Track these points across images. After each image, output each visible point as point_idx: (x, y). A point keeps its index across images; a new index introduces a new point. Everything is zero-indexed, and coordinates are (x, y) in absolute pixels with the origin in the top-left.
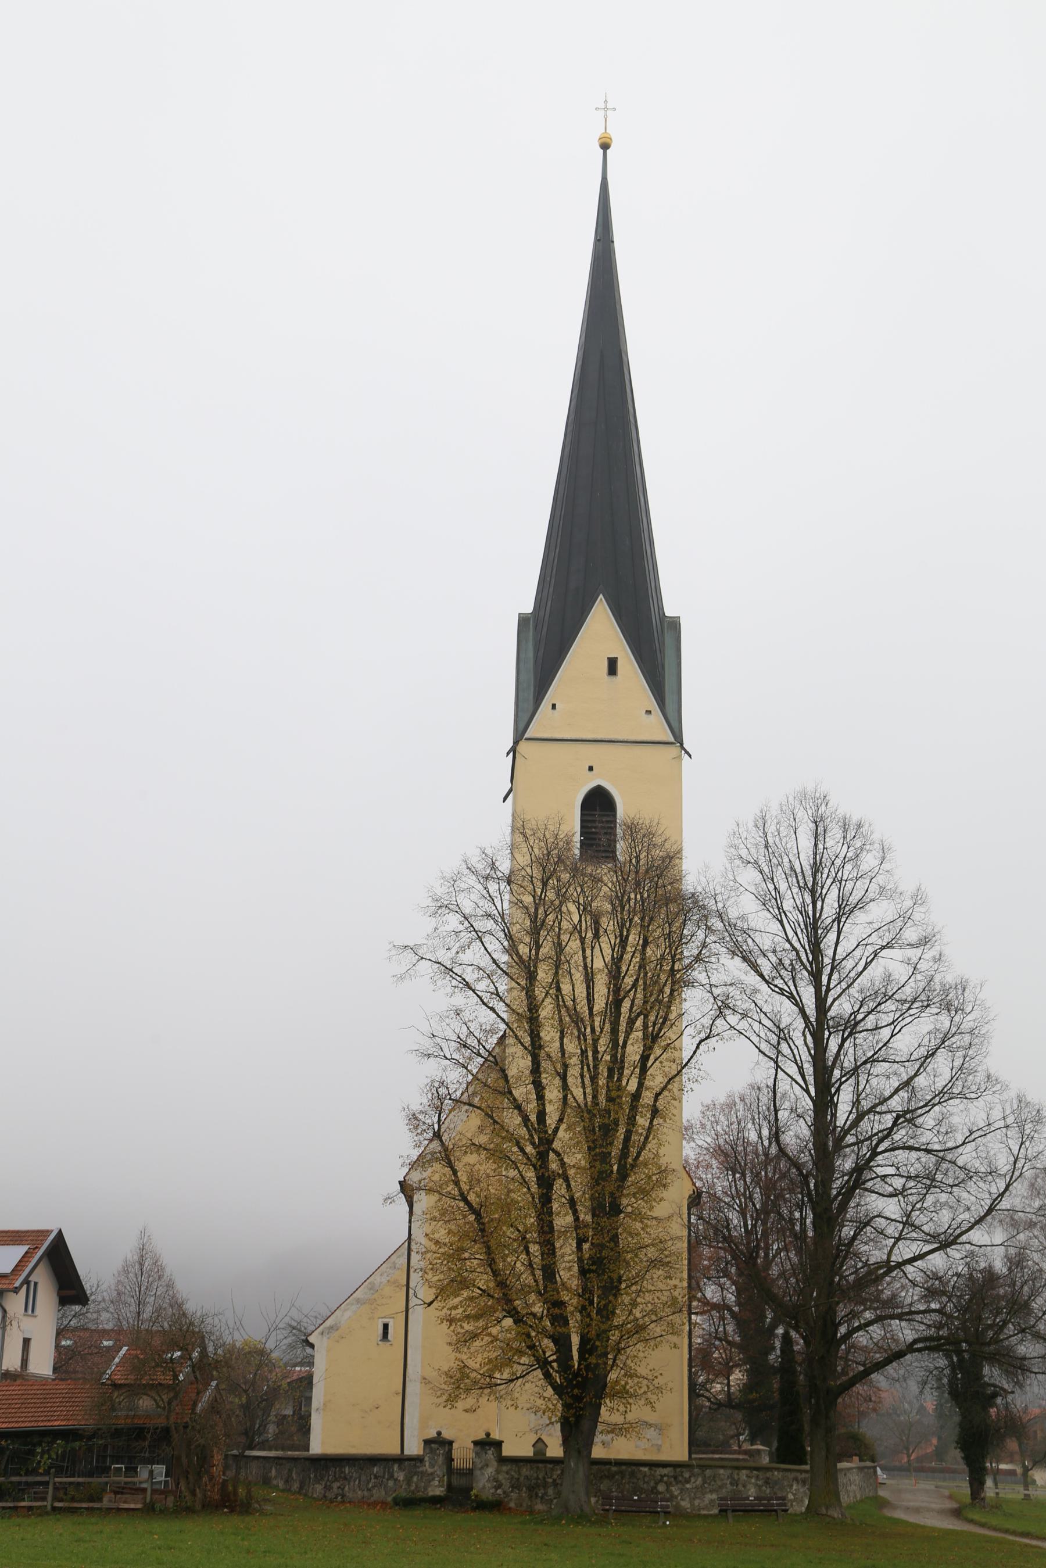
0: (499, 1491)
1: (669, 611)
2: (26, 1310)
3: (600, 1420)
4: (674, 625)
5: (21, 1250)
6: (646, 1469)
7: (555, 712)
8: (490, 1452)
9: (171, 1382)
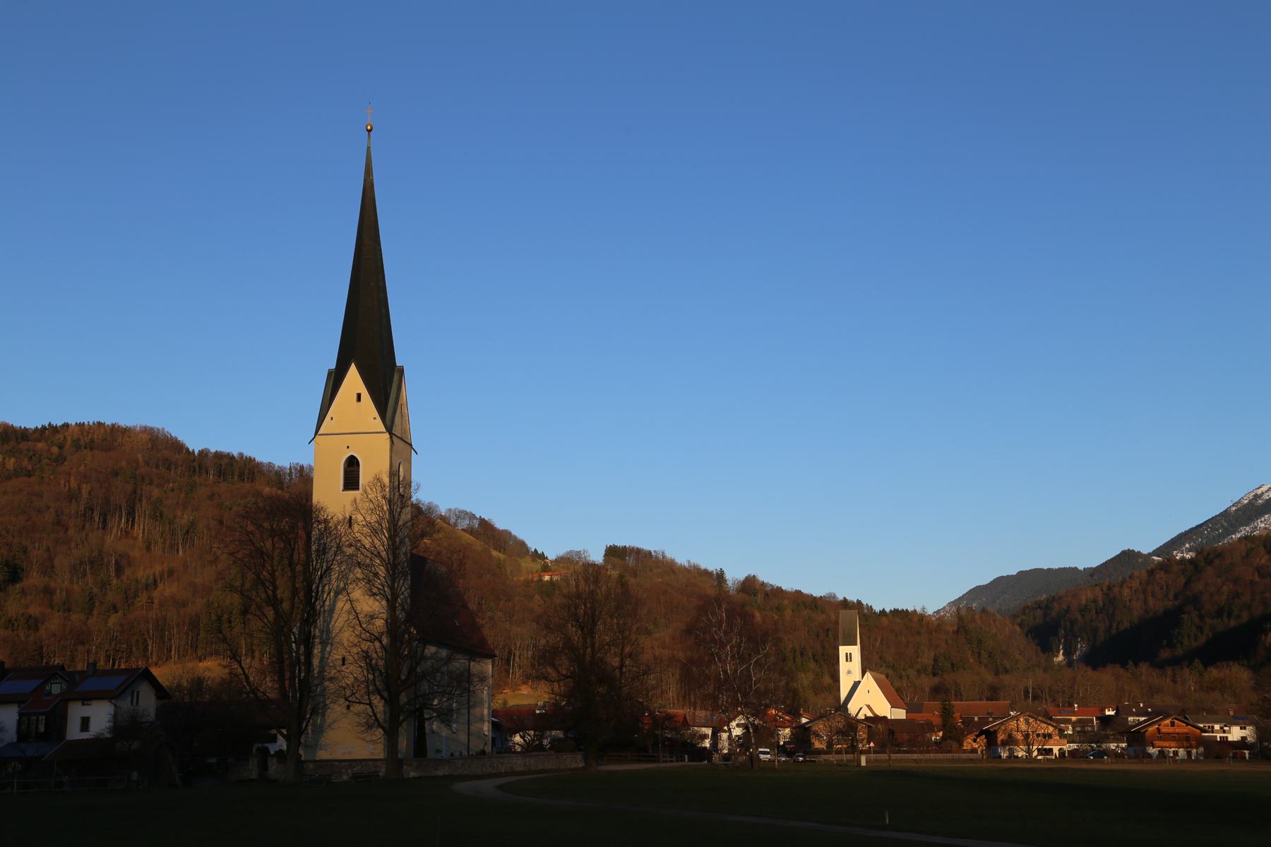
4: (401, 371)
6: (336, 763)
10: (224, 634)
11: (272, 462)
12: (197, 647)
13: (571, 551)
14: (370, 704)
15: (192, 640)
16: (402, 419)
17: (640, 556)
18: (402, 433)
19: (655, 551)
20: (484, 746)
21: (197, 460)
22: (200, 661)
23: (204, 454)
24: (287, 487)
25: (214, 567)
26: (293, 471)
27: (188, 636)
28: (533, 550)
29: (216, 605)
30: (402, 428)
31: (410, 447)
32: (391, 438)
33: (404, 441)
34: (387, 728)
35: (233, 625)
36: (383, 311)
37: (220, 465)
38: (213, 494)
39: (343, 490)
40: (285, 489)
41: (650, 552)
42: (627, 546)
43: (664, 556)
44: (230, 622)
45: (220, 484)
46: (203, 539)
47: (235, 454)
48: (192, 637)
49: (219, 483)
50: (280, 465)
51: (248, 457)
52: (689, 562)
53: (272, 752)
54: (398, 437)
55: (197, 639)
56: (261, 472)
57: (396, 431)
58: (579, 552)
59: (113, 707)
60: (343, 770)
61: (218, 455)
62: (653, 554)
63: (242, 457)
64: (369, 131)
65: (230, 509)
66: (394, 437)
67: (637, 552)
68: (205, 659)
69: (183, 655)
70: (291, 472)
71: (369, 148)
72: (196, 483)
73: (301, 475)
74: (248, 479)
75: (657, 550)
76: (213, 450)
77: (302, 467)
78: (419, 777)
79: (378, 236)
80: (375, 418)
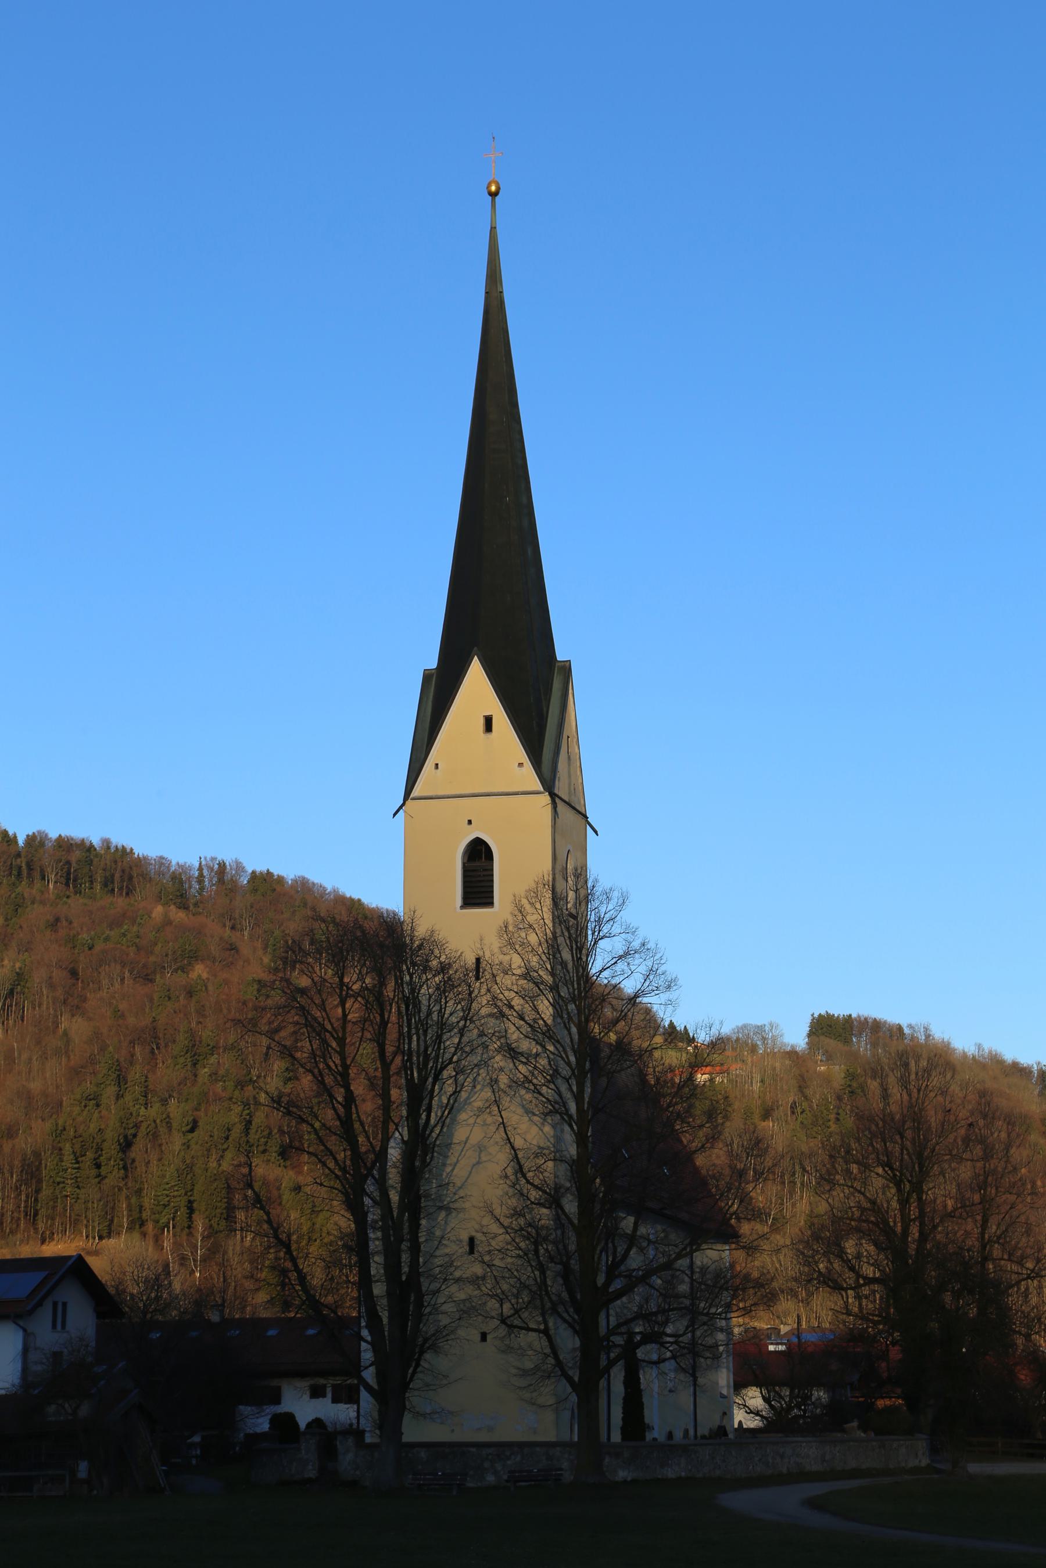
0: (358, 1473)
1: (561, 656)
2: (54, 1326)
3: (574, 1393)
4: (566, 670)
5: (39, 1276)
6: (473, 1450)
7: (438, 771)
8: (350, 1440)
9: (670, 1313)
10: (257, 1189)
11: (165, 856)
12: (36, 1214)
13: (745, 1026)
14: (546, 1332)
15: (26, 1201)
16: (569, 765)
17: (881, 1034)
18: (570, 793)
19: (910, 1026)
20: (722, 1419)
21: (23, 854)
22: (43, 1242)
23: (36, 841)
24: (196, 905)
25: (64, 1060)
26: (205, 872)
27: (20, 1194)
28: (667, 1024)
29: (72, 1133)
30: (570, 785)
31: (584, 821)
32: (554, 803)
33: (574, 808)
34: (576, 1379)
35: (104, 1171)
36: (530, 551)
37: (68, 863)
38: (57, 920)
39: (462, 907)
40: (191, 907)
41: (900, 1028)
42: (854, 1016)
43: (928, 1036)
44: (98, 1166)
45: (69, 901)
46: (40, 1005)
47: (96, 841)
48: (27, 1196)
49: (68, 897)
50: (181, 862)
51: (120, 846)
52: (979, 1047)
53: (302, 1425)
54: (565, 802)
55: (36, 1200)
56: (145, 877)
57: (561, 789)
58: (760, 1029)
59: (20, 1335)
60: (486, 1465)
61: (64, 845)
62: (906, 1031)
63: (109, 848)
64: (493, 195)
65: (90, 949)
66: (561, 806)
67: (876, 1027)
68: (52, 1239)
69: (11, 1232)
70: (201, 875)
71: (493, 229)
72: (24, 898)
73: (221, 881)
74: (121, 889)
75: (913, 1023)
76: (53, 835)
77: (222, 866)
78: (634, 1481)
79: (515, 405)
80: (521, 765)
